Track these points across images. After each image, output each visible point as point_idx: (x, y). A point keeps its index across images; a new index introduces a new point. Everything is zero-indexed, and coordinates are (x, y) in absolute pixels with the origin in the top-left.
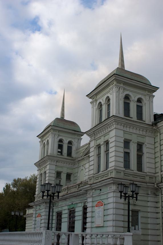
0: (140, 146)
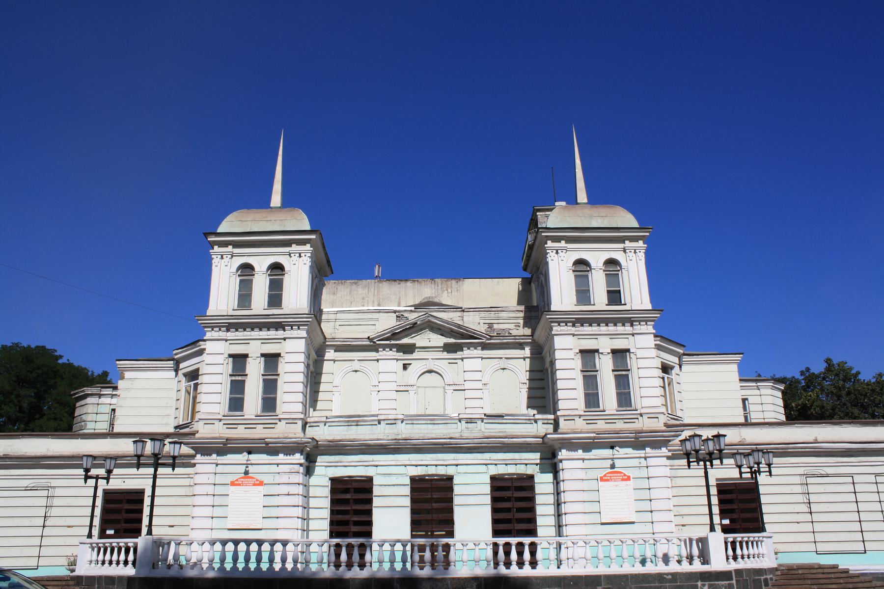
0: (620, 354)
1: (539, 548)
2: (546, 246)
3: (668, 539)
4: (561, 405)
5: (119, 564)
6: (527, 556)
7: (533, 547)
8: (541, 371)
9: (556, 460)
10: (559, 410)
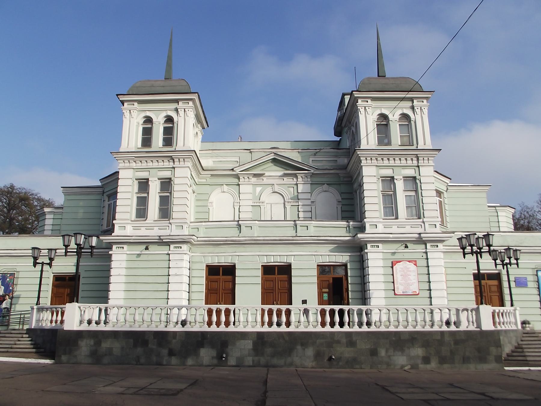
1: (292, 313)
2: (357, 104)
3: (449, 308)
4: (174, 215)
5: (211, 324)
6: (284, 318)
7: (288, 312)
8: (352, 193)
9: (363, 253)
10: (366, 218)
